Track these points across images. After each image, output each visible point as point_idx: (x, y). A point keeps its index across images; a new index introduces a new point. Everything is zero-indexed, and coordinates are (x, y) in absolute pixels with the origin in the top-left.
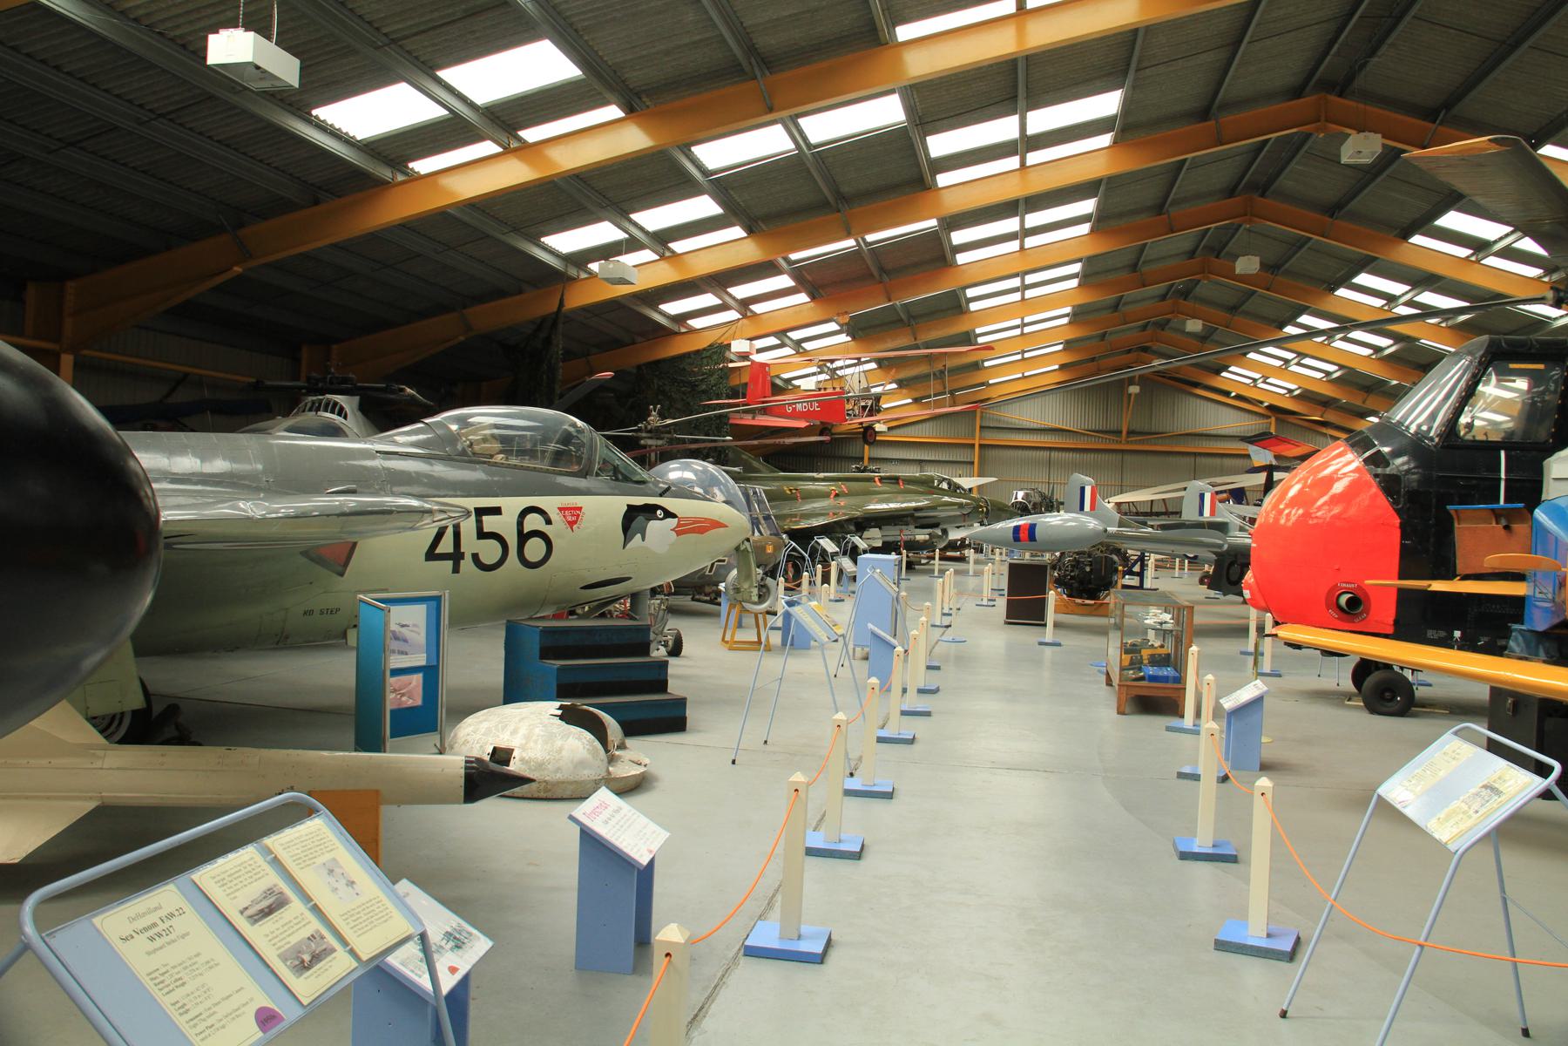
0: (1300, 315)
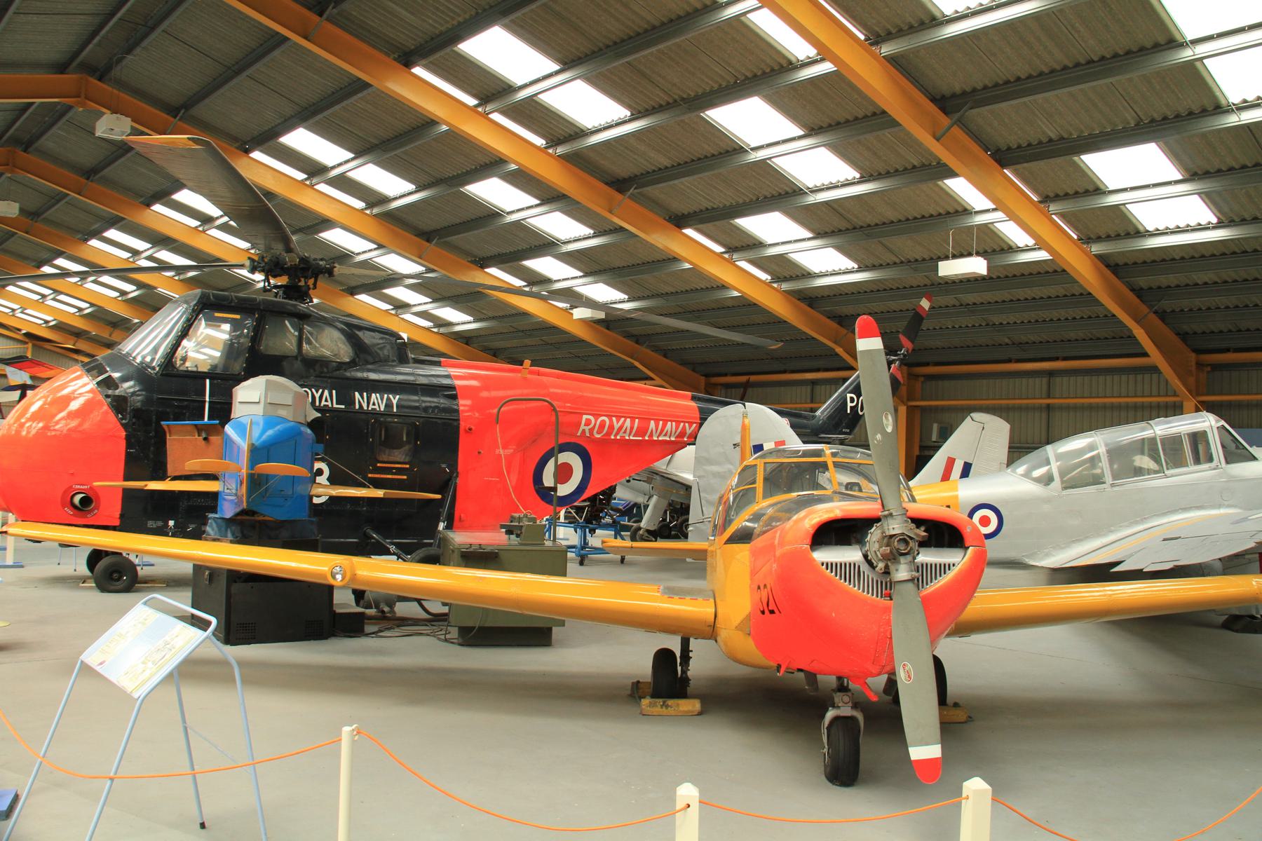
0: (55, 258)
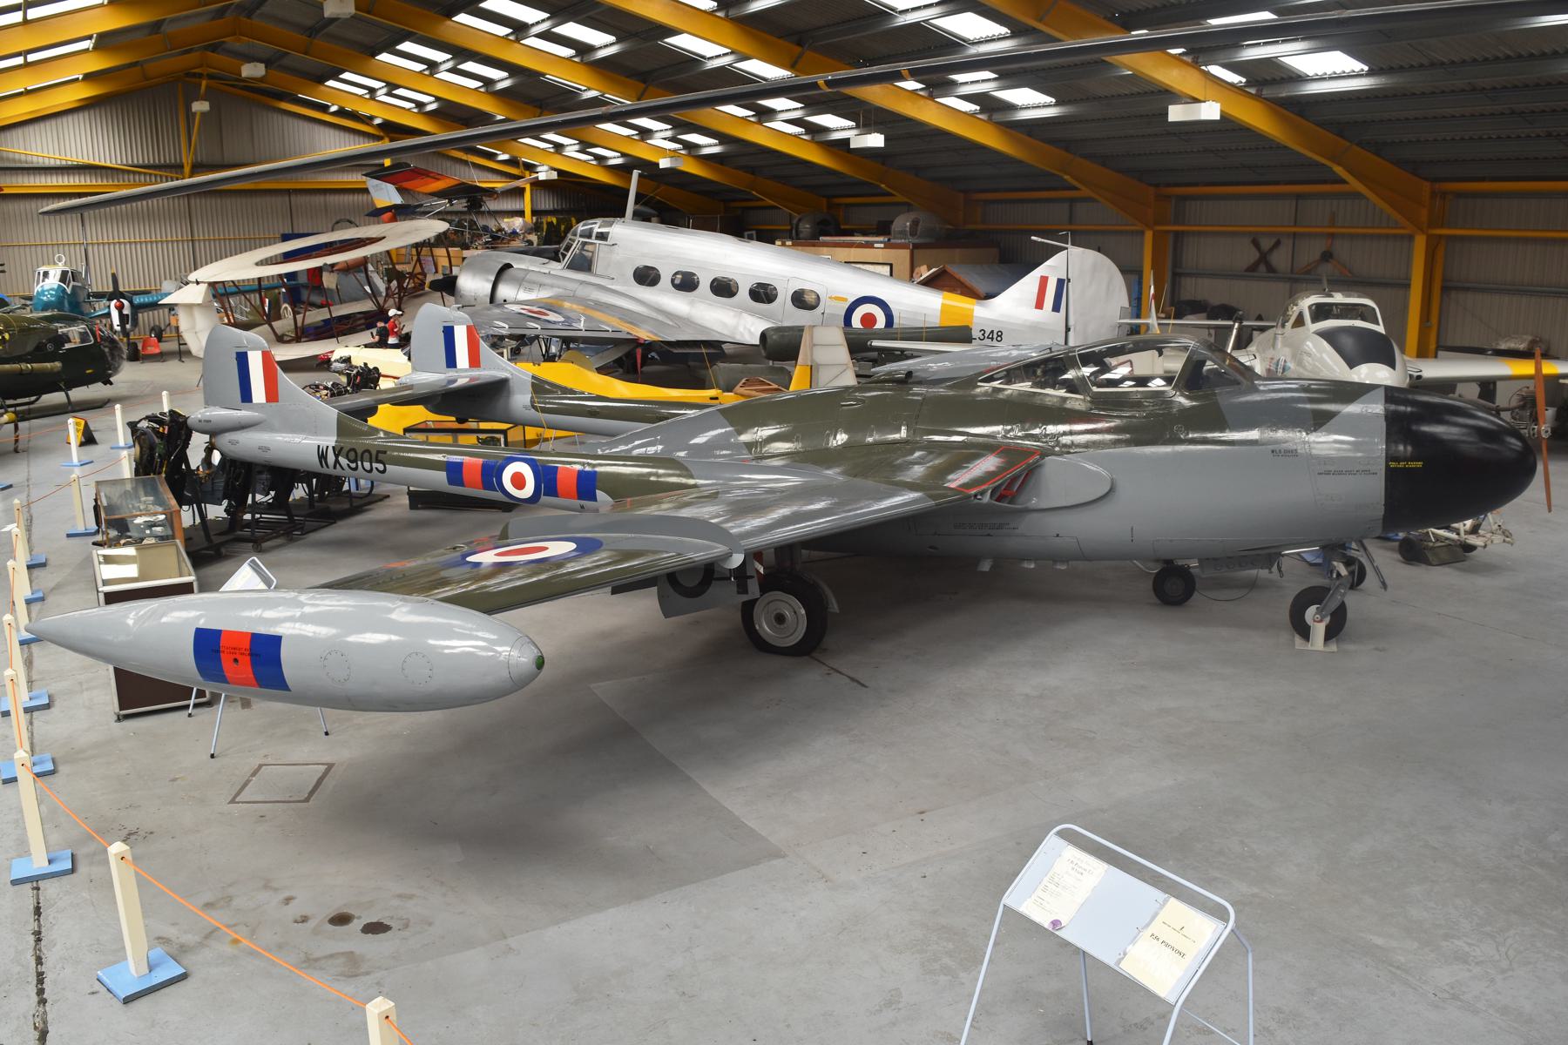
0: (343, 71)
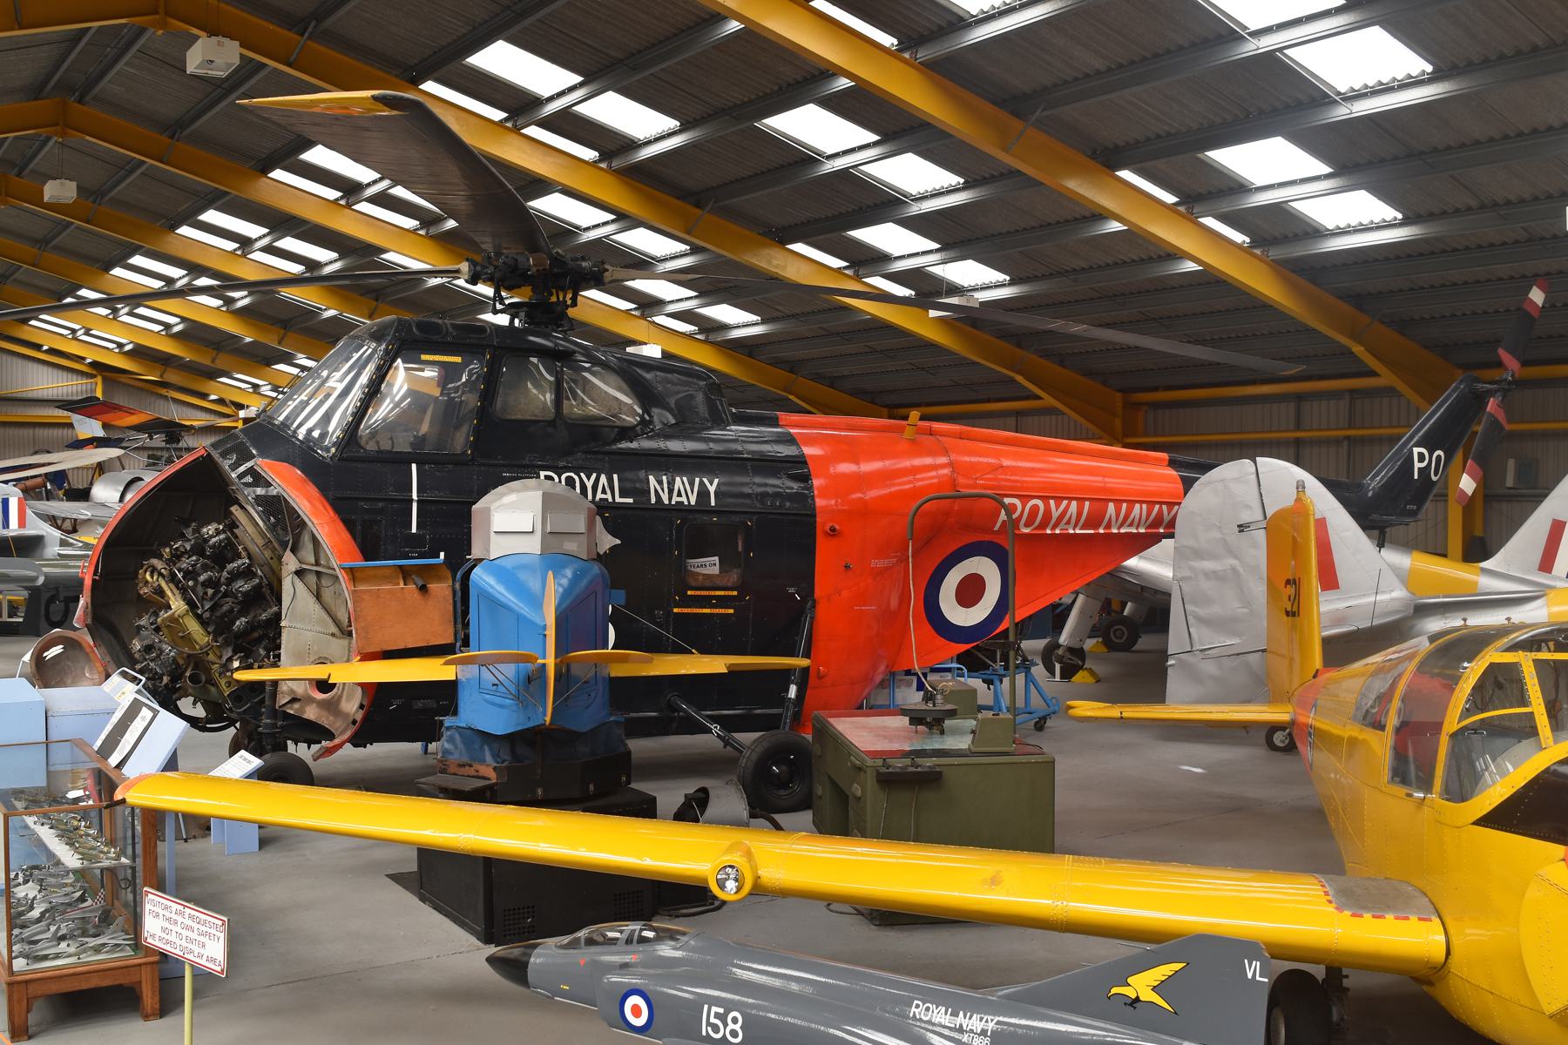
0: (131, 255)
